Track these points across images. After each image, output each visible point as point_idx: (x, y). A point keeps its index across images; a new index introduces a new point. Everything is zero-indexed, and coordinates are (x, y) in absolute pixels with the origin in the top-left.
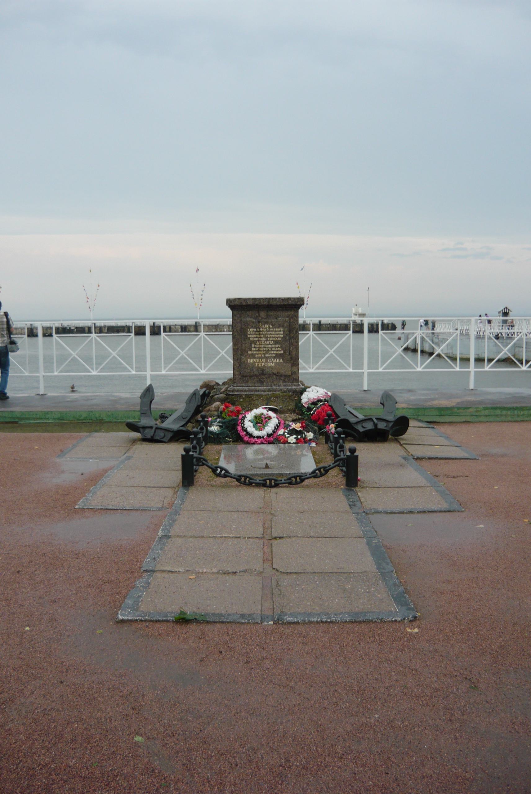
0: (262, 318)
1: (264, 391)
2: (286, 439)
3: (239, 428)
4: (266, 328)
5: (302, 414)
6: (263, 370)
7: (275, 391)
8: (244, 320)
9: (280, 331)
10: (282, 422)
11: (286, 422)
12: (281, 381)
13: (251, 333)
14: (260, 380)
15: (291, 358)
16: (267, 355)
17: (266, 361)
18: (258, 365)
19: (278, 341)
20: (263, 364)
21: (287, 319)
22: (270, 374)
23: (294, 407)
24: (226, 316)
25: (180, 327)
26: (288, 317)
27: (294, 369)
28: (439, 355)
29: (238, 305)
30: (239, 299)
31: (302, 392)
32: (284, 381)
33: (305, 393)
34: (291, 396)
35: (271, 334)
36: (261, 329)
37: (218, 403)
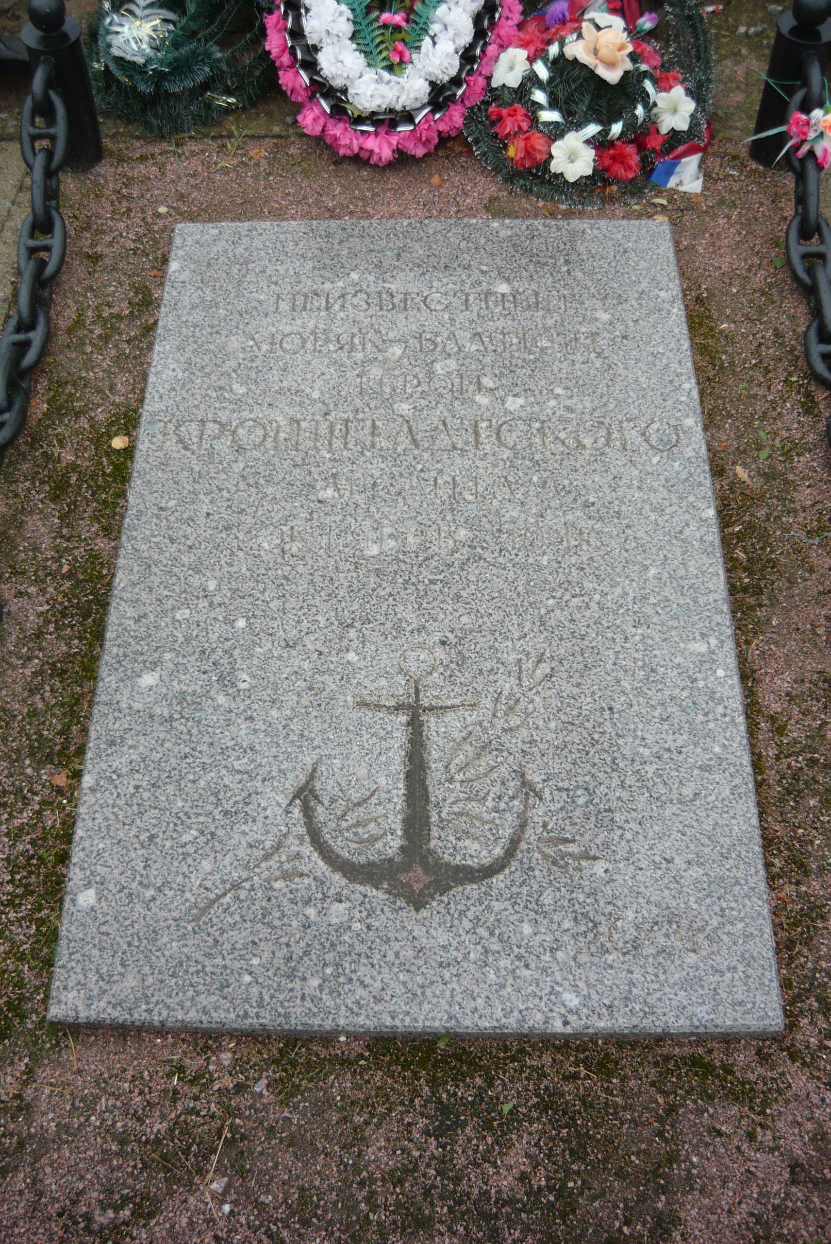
2: (539, 142)
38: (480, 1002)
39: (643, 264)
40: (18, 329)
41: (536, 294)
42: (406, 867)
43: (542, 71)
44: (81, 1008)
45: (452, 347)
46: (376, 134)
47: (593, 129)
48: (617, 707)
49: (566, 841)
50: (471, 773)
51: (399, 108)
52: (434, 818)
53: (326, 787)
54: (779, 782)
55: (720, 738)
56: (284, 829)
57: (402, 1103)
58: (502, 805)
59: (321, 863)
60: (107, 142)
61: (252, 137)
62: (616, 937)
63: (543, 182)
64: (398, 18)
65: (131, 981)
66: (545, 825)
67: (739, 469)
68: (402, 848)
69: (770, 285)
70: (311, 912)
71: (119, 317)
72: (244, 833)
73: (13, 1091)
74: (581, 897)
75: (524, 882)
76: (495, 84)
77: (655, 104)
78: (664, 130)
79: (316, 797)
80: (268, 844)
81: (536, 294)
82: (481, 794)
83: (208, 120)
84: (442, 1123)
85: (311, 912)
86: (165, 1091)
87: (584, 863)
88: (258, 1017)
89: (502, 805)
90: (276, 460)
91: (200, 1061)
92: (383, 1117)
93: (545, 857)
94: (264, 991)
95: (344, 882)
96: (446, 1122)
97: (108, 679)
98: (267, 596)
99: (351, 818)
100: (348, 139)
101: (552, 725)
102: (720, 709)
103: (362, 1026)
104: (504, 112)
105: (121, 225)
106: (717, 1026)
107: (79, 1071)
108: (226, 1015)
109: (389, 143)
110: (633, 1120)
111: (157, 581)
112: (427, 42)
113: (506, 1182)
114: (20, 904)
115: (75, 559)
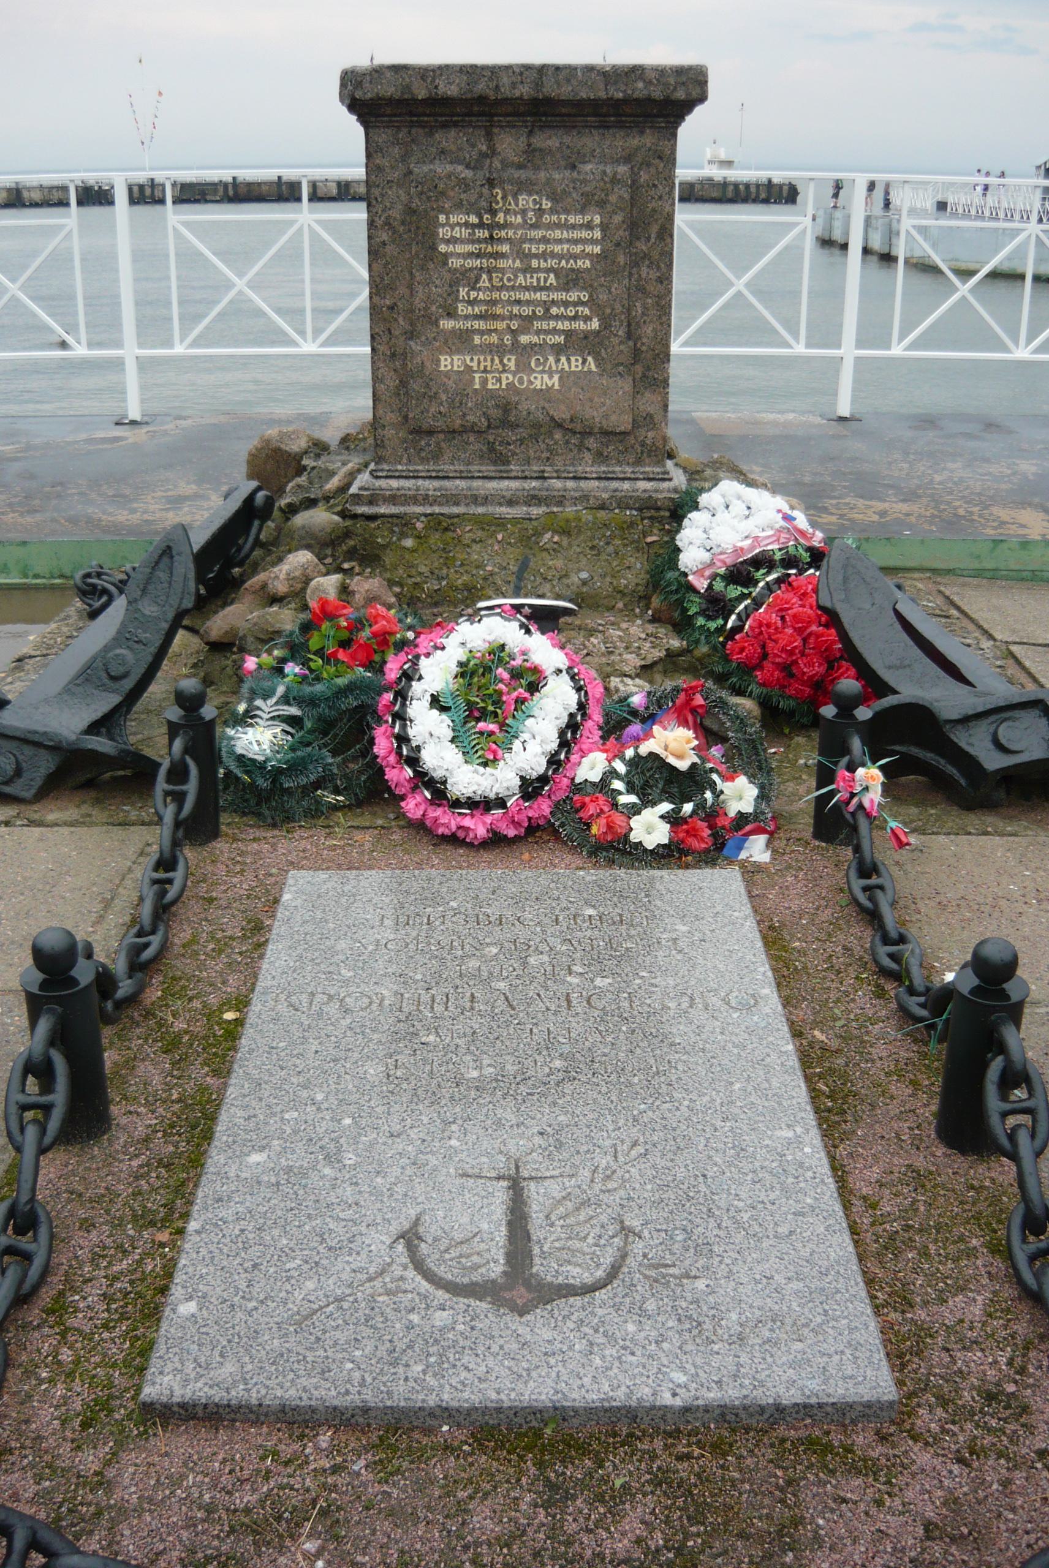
0: (505, 164)
1: (511, 503)
2: (619, 819)
3: (382, 746)
4: (524, 212)
5: (682, 625)
6: (506, 408)
7: (560, 503)
8: (421, 170)
9: (589, 226)
10: (596, 690)
11: (615, 681)
12: (588, 457)
13: (454, 232)
14: (492, 450)
15: (636, 353)
16: (524, 339)
17: (523, 367)
18: (484, 382)
19: (578, 271)
20: (507, 378)
21: (622, 169)
22: (537, 426)
23: (644, 577)
24: (341, 146)
25: (334, 185)
26: (627, 159)
27: (648, 402)
28: (966, 274)
29: (390, 101)
30: (397, 69)
31: (678, 511)
32: (600, 457)
33: (693, 515)
34: (632, 525)
35: (545, 240)
36: (500, 217)
37: (303, 557)
38: (587, 1381)
39: (716, 896)
40: (139, 935)
41: (621, 915)
42: (509, 1287)
43: (620, 767)
44: (176, 1387)
45: (544, 947)
46: (472, 816)
47: (666, 807)
48: (710, 1174)
49: (666, 1266)
50: (571, 1220)
51: (492, 796)
52: (536, 1250)
53: (430, 1229)
54: (876, 1241)
55: (812, 1193)
56: (388, 1260)
57: (508, 1482)
58: (602, 1242)
59: (424, 1283)
60: (223, 828)
61: (358, 828)
62: (720, 1332)
63: (624, 852)
64: (492, 727)
65: (230, 1367)
66: (645, 1256)
67: (816, 1033)
68: (505, 1273)
69: (837, 919)
70: (415, 1318)
71: (231, 938)
72: (348, 1262)
73: (96, 1467)
74: (684, 1305)
75: (626, 1295)
76: (577, 781)
77: (722, 792)
78: (732, 814)
79: (420, 1238)
80: (372, 1270)
81: (621, 915)
82: (582, 1235)
83: (317, 813)
84: (550, 1497)
85: (415, 1318)
86: (258, 1471)
87: (685, 1281)
88: (359, 1393)
89: (602, 1242)
90: (381, 1018)
91: (296, 1446)
92: (486, 1495)
93: (646, 1277)
94: (367, 1375)
95: (447, 1296)
96: (555, 1496)
97: (216, 1157)
98: (372, 1103)
99: (454, 1253)
100: (447, 820)
101: (649, 1187)
102: (810, 1174)
103: (466, 1401)
104: (587, 799)
105: (234, 880)
106: (829, 1396)
107: (166, 1454)
108: (326, 1393)
109: (484, 823)
110: (752, 1491)
111: (267, 1094)
112: (517, 745)
113: (622, 1546)
114: (114, 1327)
115: (185, 1090)
